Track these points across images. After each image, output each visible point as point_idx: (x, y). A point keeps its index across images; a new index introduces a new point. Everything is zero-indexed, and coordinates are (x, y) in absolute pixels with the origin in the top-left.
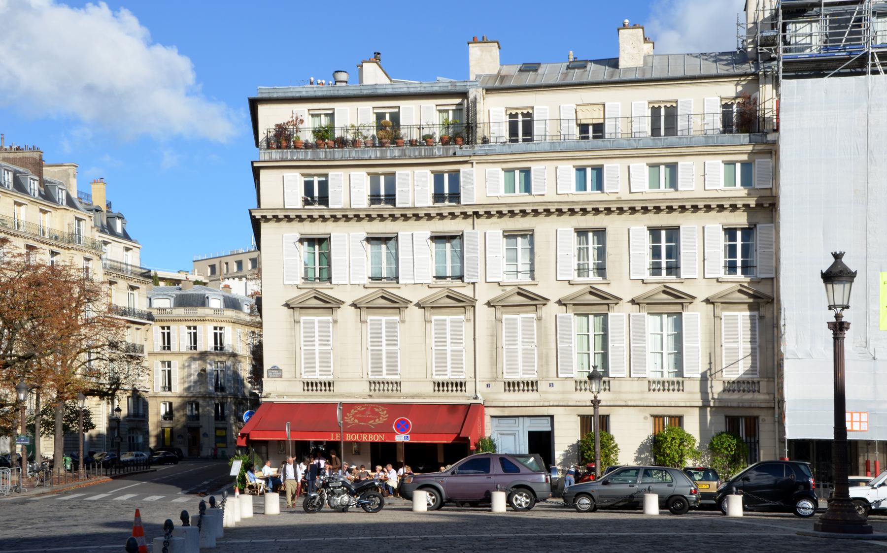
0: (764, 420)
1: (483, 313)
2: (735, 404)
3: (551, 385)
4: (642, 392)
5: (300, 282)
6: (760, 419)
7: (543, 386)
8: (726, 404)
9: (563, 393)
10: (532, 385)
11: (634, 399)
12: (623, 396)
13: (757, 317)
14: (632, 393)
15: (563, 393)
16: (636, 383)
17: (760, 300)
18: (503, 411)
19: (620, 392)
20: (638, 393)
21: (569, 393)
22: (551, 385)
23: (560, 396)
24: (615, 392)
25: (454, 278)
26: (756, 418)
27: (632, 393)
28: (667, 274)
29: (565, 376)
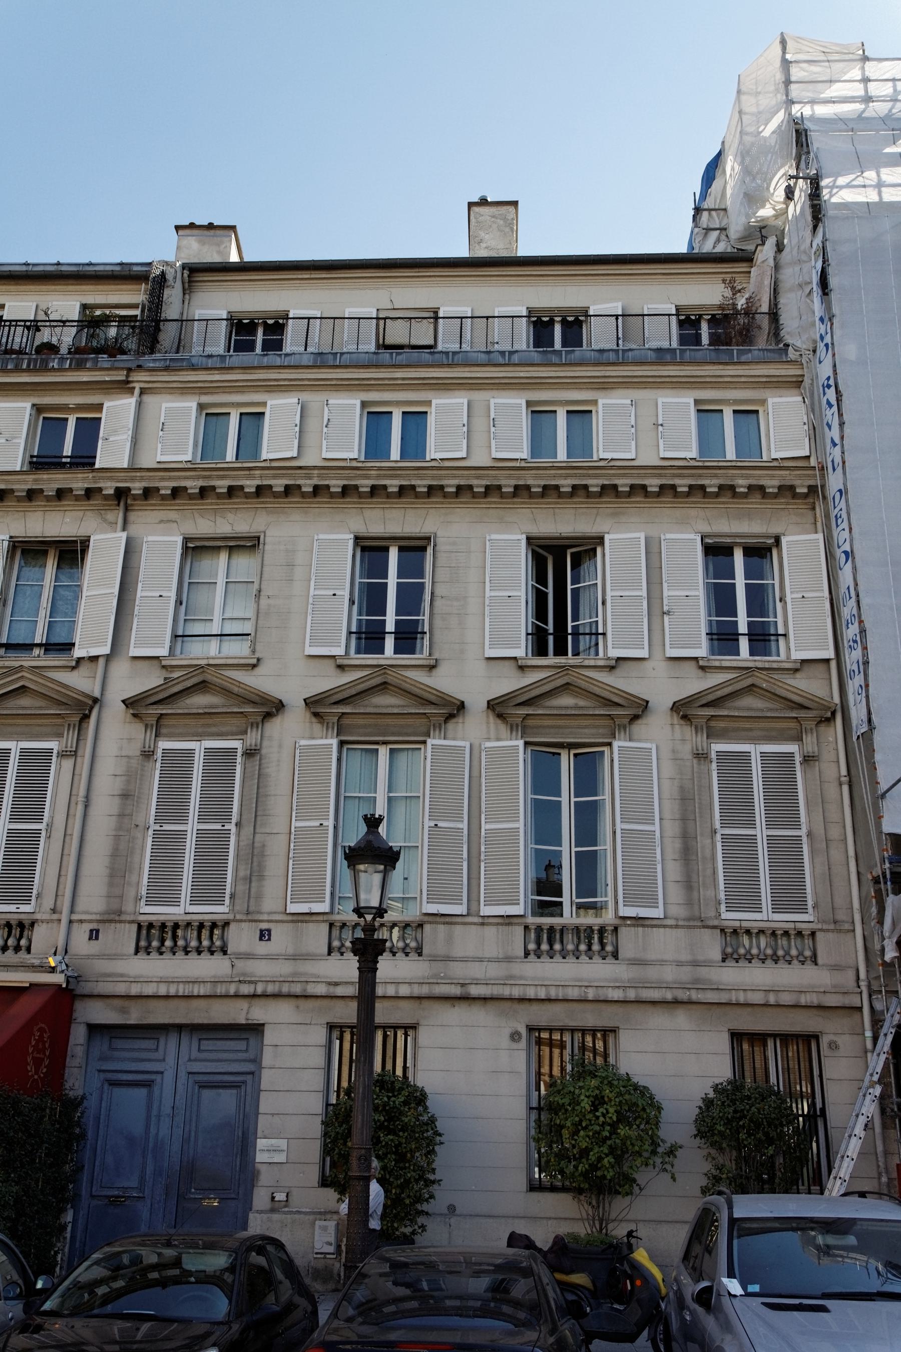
0: (833, 1046)
1: (116, 734)
2: (757, 998)
3: (265, 935)
4: (508, 959)
5: (520, 649)
6: (824, 1041)
7: (241, 938)
8: (734, 997)
9: (295, 958)
10: (209, 936)
11: (482, 975)
12: (459, 971)
13: (798, 759)
14: (481, 960)
15: (295, 958)
16: (490, 932)
17: (802, 714)
18: (124, 1011)
19: (448, 959)
20: (498, 960)
21: (707, 964)
22: (265, 935)
23: (283, 969)
24: (434, 959)
25: (49, 647)
26: (809, 1039)
27: (481, 960)
28: (397, 651)
29: (303, 908)
